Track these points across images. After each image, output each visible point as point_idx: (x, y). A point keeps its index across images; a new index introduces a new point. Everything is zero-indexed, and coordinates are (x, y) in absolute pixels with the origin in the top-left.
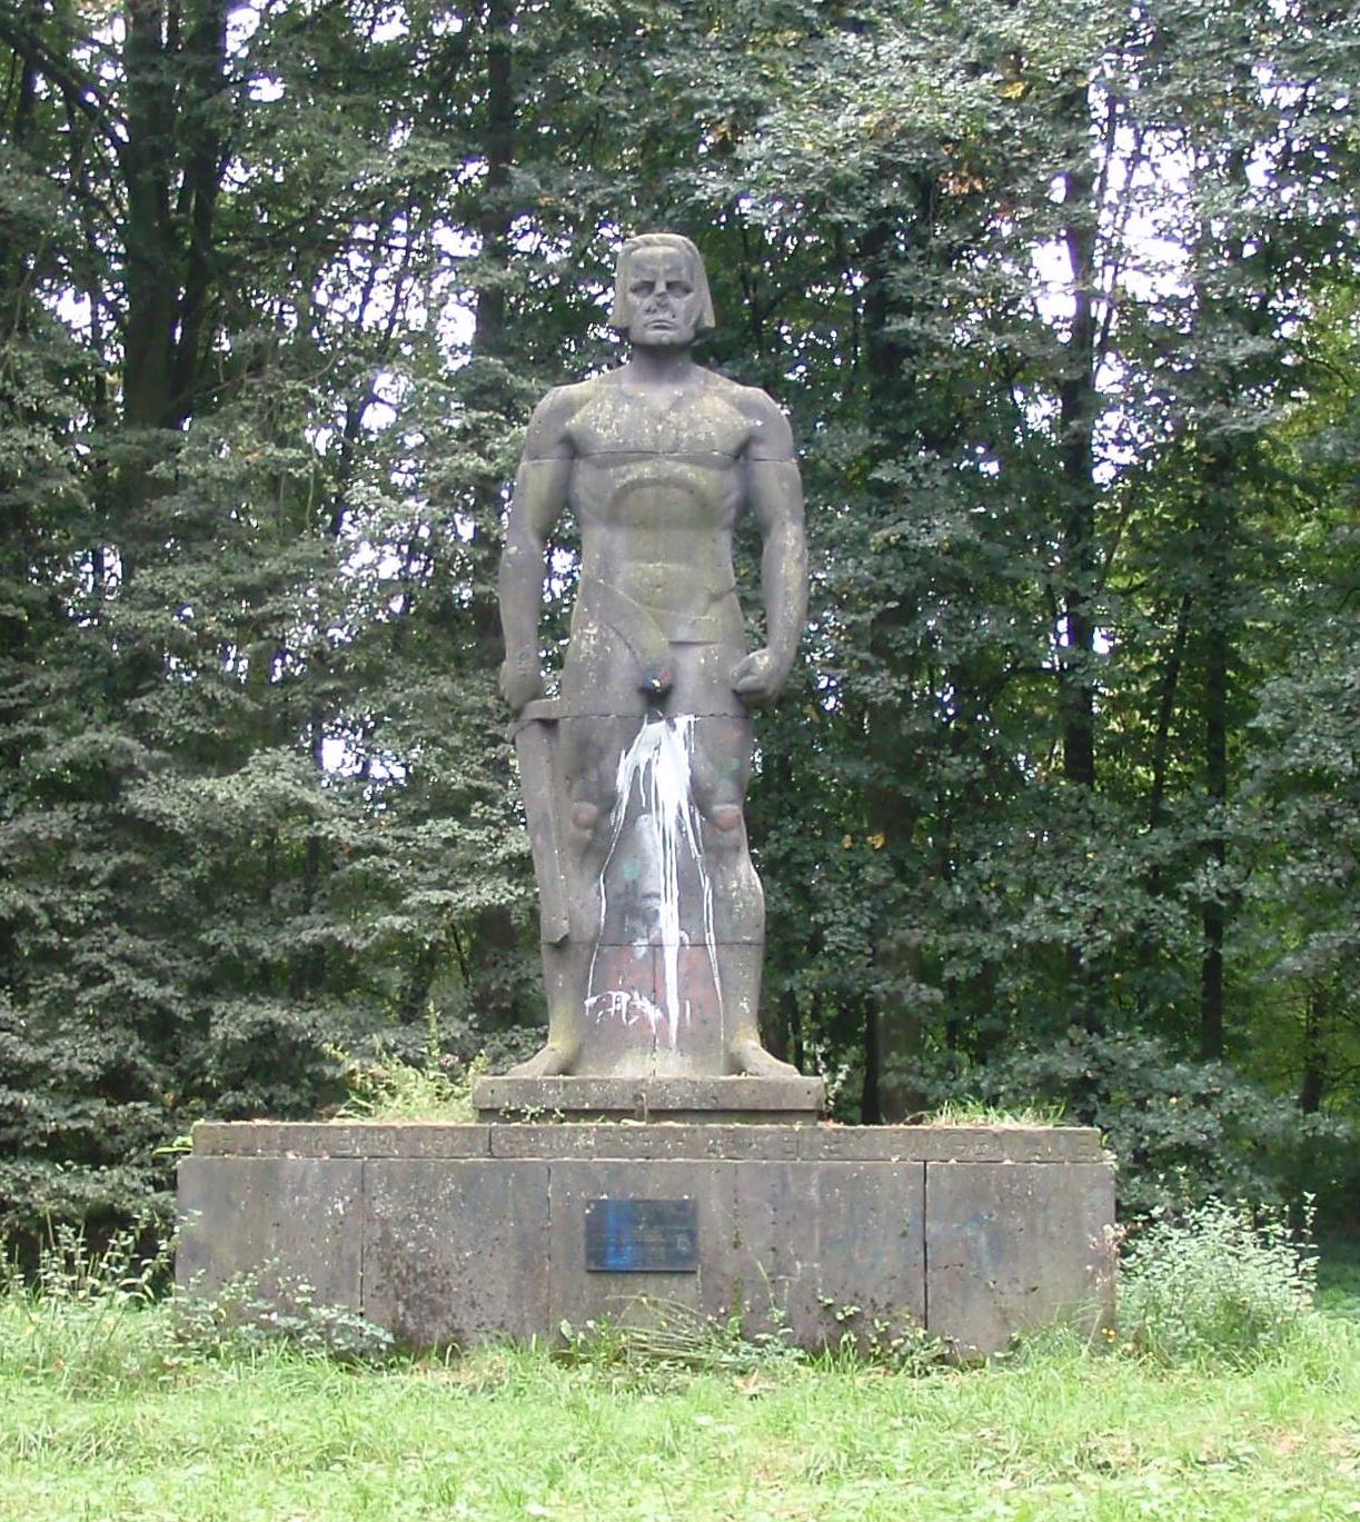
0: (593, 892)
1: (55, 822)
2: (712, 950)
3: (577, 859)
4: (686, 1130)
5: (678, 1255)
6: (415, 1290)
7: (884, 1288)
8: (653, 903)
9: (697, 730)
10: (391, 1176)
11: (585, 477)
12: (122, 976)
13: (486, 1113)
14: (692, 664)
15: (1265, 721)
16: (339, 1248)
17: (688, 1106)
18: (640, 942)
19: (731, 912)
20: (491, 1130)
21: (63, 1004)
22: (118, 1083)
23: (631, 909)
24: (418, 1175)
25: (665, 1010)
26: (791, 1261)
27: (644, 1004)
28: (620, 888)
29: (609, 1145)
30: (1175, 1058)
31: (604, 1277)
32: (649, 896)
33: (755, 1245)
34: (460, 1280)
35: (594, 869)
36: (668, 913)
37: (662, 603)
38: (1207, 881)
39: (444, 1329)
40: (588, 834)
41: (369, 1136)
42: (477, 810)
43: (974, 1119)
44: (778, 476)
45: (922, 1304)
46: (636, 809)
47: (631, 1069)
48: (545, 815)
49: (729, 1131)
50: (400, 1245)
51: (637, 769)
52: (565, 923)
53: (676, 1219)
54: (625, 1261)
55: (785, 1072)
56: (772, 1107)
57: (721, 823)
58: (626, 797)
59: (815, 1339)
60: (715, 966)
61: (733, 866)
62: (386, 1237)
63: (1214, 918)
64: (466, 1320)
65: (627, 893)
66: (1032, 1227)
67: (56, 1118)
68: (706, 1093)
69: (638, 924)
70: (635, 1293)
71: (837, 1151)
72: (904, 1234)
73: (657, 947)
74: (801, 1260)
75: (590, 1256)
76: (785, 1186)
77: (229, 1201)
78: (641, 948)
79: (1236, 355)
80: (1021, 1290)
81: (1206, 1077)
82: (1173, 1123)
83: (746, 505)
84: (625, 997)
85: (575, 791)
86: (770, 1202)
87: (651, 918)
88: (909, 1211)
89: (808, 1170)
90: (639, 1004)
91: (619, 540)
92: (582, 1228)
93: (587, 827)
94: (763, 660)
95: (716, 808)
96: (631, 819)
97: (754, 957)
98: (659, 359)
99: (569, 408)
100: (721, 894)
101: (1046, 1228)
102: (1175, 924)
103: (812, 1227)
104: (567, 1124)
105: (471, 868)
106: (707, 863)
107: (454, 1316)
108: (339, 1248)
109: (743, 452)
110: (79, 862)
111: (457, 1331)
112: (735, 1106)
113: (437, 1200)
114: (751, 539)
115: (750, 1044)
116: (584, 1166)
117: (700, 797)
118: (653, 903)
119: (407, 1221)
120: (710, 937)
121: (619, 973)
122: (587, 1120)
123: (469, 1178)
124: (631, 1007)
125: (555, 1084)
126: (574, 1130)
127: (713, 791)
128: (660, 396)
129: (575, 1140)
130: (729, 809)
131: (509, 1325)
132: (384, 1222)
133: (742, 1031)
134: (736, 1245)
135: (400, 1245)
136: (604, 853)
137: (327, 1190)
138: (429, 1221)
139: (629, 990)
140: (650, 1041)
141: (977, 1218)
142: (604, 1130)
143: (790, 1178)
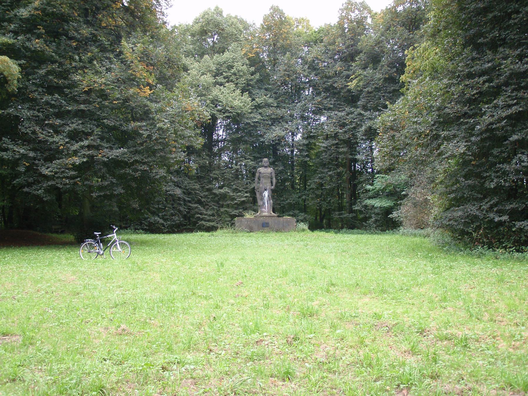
1: (207, 193)
9: (268, 192)
11: (261, 175)
12: (213, 206)
14: (268, 187)
15: (308, 184)
21: (208, 209)
22: (213, 215)
23: (264, 203)
29: (263, 219)
30: (300, 212)
36: (266, 204)
37: (266, 183)
38: (304, 197)
42: (242, 192)
43: (287, 217)
44: (274, 175)
47: (264, 214)
53: (268, 223)
63: (304, 201)
67: (208, 218)
79: (305, 154)
81: (303, 214)
82: (300, 218)
83: (271, 176)
91: (263, 179)
94: (273, 187)
98: (266, 167)
99: (260, 170)
102: (301, 202)
105: (242, 197)
109: (271, 173)
110: (209, 196)
114: (272, 178)
117: (268, 196)
123: (254, 221)
128: (266, 169)
130: (270, 197)
140: (265, 212)
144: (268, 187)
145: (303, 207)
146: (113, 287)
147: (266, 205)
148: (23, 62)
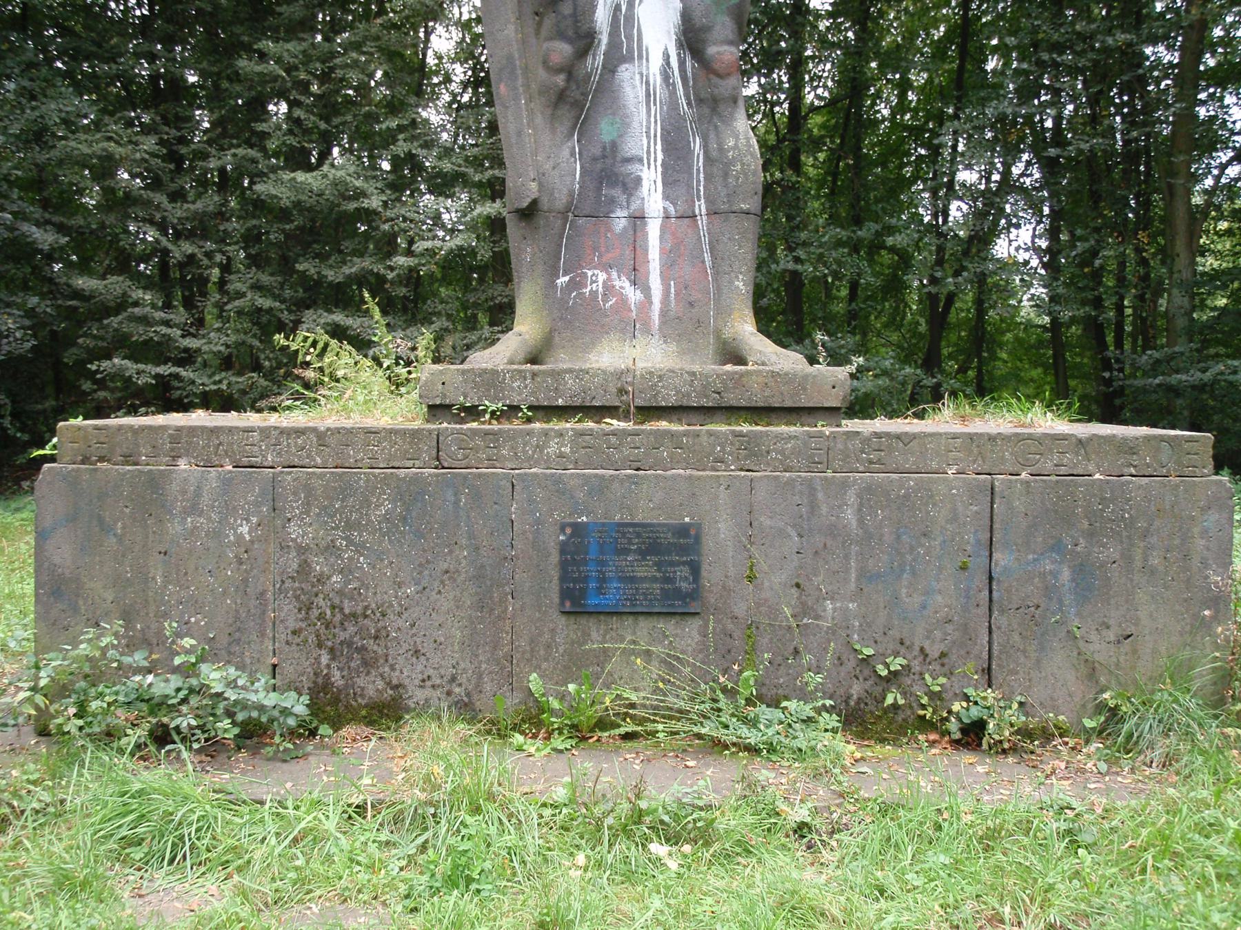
0: (566, 153)
2: (702, 222)
3: (549, 112)
4: (686, 434)
5: (679, 594)
6: (343, 636)
7: (938, 634)
8: (633, 168)
10: (309, 490)
13: (437, 410)
16: (245, 581)
17: (685, 403)
18: (619, 213)
19: (726, 175)
20: (712, 213)
24: (344, 490)
25: (647, 291)
26: (820, 599)
27: (623, 284)
28: (597, 151)
29: (589, 451)
31: (583, 620)
32: (629, 160)
33: (775, 580)
34: (400, 623)
35: (568, 124)
36: (651, 178)
39: (380, 684)
40: (560, 80)
41: (283, 439)
45: (985, 655)
46: (618, 56)
48: (510, 58)
49: (740, 435)
50: (322, 579)
51: (617, 8)
52: (534, 185)
54: (614, 595)
55: (789, 360)
56: (788, 404)
57: (716, 66)
58: (604, 39)
59: (849, 697)
60: (705, 240)
61: (728, 120)
62: (304, 568)
64: (408, 673)
65: (604, 157)
66: (1128, 558)
68: (704, 387)
69: (617, 192)
70: (622, 640)
71: (879, 462)
72: (964, 568)
73: (638, 219)
74: (832, 599)
75: (565, 594)
76: (813, 507)
77: (101, 520)
78: (620, 220)
80: (1112, 638)
84: (602, 277)
85: (549, 22)
86: (794, 526)
87: (631, 186)
88: (972, 537)
89: (844, 485)
90: (617, 283)
92: (555, 558)
93: (559, 70)
95: (712, 50)
96: (610, 68)
97: (751, 227)
100: (714, 154)
101: (1146, 560)
103: (847, 557)
104: (537, 425)
106: (699, 120)
107: (393, 668)
108: (245, 581)
111: (397, 687)
112: (743, 403)
113: (369, 521)
115: (745, 329)
116: (558, 480)
118: (633, 168)
119: (331, 549)
120: (701, 207)
121: (595, 249)
122: (560, 418)
123: (411, 493)
124: (608, 288)
125: (521, 375)
126: (546, 433)
127: (707, 29)
129: (546, 445)
131: (462, 679)
132: (302, 550)
133: (736, 315)
134: (751, 579)
135: (322, 579)
136: (578, 106)
137: (229, 510)
138: (360, 548)
139: (607, 267)
141: (1057, 547)
142: (582, 434)
143: (820, 495)
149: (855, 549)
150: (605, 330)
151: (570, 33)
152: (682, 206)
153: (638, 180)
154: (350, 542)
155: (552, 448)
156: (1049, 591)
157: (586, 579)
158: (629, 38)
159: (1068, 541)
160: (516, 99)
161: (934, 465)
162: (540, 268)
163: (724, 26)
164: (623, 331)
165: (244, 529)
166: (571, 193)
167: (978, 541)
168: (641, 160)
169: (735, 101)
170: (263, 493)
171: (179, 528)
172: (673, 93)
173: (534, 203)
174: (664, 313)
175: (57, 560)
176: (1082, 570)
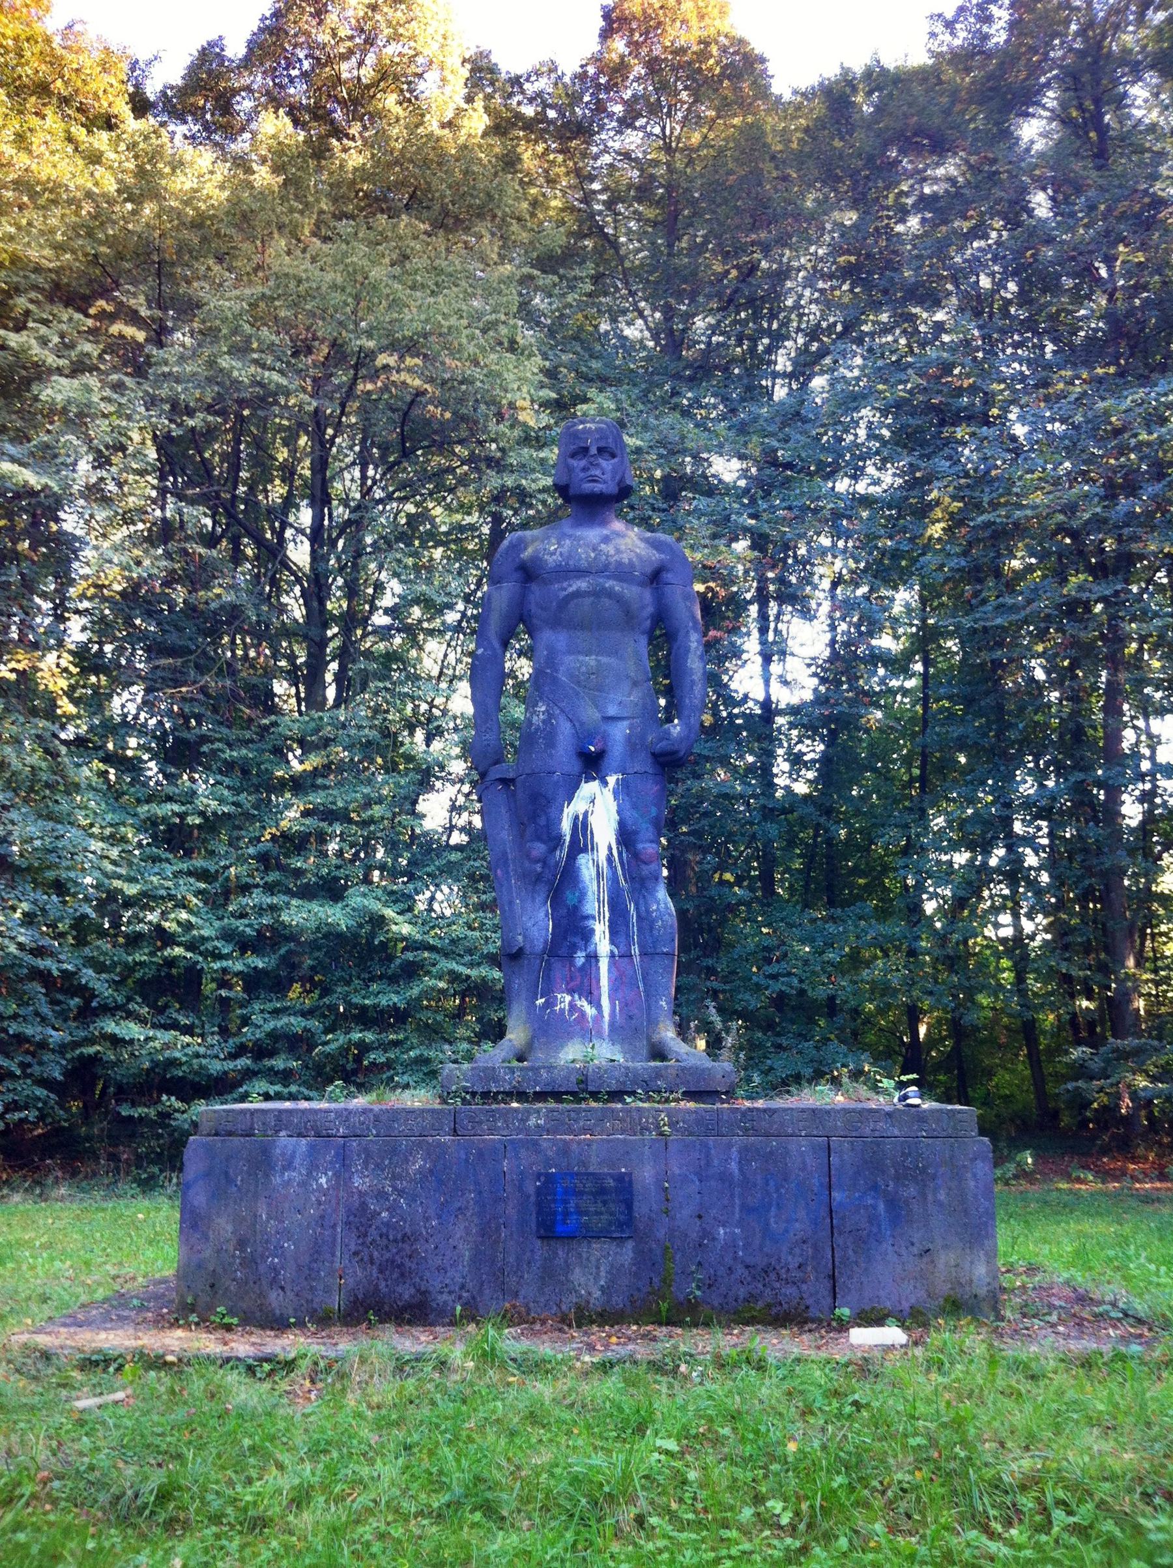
0: (542, 914)
2: (637, 960)
20: (643, 954)
25: (599, 1007)
27: (583, 1004)
31: (552, 1243)
33: (684, 1215)
36: (601, 932)
45: (830, 1265)
47: (572, 1053)
48: (505, 854)
52: (520, 938)
58: (568, 838)
64: (435, 1283)
73: (593, 958)
78: (580, 958)
84: (568, 998)
87: (587, 935)
90: (579, 1003)
100: (644, 914)
103: (732, 1196)
106: (633, 891)
117: (625, 836)
120: (635, 950)
127: (636, 833)
129: (528, 1119)
133: (661, 1025)
138: (401, 1193)
140: (585, 1030)
141: (875, 1187)
142: (552, 1111)
144: (619, 732)
145: (631, 280)
146: (678, 79)
147: (602, 943)
148: (54, 527)
149: (737, 1190)
150: (570, 1036)
151: (545, 837)
152: (623, 949)
153: (592, 931)
154: (395, 1188)
155: (532, 1122)
156: (873, 1219)
157: (555, 1213)
158: (585, 835)
159: (881, 1183)
160: (508, 880)
161: (790, 1131)
162: (524, 995)
163: (646, 830)
164: (583, 1037)
165: (323, 1180)
166: (546, 942)
167: (821, 1185)
168: (594, 918)
169: (657, 879)
170: (337, 1154)
171: (279, 1180)
172: (615, 873)
173: (521, 949)
174: (612, 1024)
175: (196, 1203)
176: (893, 1204)
